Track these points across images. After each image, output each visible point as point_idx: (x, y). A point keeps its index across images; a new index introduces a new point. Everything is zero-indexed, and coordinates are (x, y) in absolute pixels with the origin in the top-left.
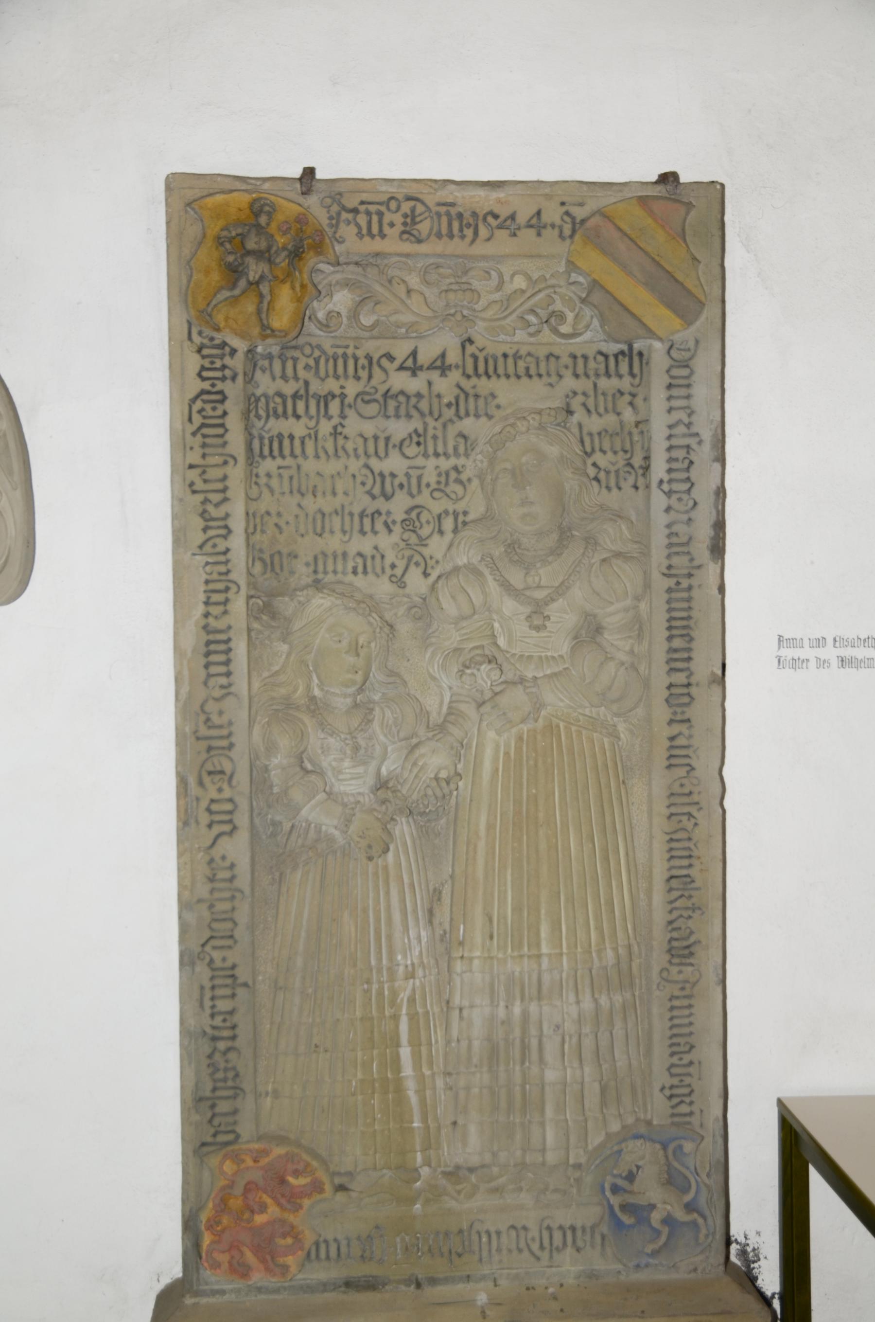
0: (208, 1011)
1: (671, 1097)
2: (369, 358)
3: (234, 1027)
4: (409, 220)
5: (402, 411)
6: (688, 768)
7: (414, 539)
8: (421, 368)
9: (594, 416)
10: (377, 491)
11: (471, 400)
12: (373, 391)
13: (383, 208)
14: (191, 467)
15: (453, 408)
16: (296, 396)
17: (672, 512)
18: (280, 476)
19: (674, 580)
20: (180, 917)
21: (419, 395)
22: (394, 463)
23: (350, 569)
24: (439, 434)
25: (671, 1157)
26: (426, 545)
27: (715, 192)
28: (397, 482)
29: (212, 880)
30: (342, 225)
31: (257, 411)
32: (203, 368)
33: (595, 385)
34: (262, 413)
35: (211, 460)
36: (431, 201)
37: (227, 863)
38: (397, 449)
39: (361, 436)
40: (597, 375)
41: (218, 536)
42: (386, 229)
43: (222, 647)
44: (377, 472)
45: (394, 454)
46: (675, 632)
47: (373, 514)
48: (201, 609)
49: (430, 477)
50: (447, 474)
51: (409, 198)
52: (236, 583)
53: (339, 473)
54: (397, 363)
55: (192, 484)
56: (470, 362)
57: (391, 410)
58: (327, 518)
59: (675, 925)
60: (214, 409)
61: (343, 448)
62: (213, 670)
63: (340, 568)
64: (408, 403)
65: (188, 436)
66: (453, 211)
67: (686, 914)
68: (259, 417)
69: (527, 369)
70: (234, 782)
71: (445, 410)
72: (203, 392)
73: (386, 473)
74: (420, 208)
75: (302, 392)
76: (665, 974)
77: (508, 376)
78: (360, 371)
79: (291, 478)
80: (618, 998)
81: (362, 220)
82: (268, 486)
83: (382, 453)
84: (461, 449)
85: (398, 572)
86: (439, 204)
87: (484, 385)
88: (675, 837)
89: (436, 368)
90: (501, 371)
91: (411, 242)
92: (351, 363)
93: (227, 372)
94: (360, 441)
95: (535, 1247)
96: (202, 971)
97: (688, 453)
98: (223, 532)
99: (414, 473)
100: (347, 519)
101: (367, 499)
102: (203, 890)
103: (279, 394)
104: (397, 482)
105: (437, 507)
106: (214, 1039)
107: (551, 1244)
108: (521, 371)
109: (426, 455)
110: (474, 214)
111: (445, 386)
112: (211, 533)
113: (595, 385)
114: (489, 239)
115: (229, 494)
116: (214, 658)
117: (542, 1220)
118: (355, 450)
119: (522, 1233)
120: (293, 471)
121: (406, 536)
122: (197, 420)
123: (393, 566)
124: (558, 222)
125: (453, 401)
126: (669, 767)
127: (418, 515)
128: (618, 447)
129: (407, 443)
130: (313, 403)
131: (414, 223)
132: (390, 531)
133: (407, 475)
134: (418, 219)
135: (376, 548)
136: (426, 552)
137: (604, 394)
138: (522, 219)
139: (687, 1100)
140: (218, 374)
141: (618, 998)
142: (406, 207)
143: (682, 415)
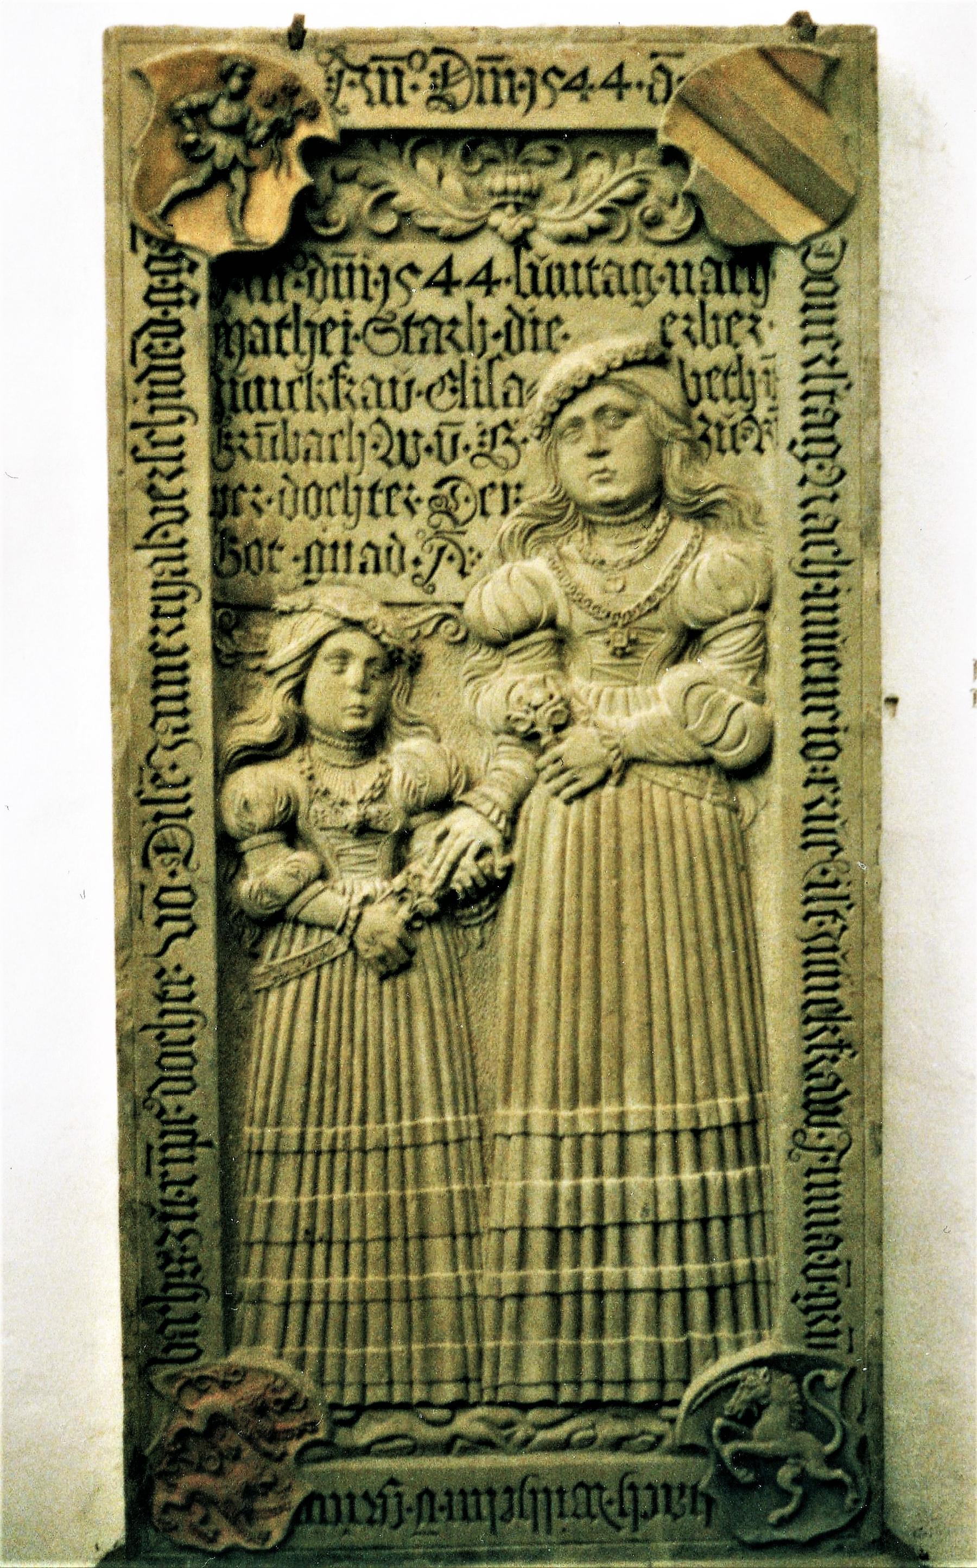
0: (158, 1180)
1: (806, 1311)
2: (384, 269)
3: (193, 1202)
4: (439, 81)
5: (431, 345)
6: (834, 848)
7: (446, 523)
8: (458, 283)
9: (701, 348)
10: (394, 455)
11: (528, 328)
12: (389, 317)
13: (403, 65)
14: (135, 425)
15: (502, 340)
16: (281, 324)
17: (808, 485)
18: (259, 435)
19: (813, 581)
20: (119, 1051)
21: (454, 322)
22: (421, 418)
23: (355, 565)
24: (483, 374)
25: (807, 1394)
26: (464, 533)
27: (863, 39)
28: (423, 443)
29: (162, 997)
30: (345, 90)
31: (228, 348)
32: (151, 290)
33: (702, 305)
34: (236, 349)
35: (160, 416)
36: (470, 53)
37: (183, 976)
38: (423, 398)
39: (372, 378)
40: (705, 291)
41: (171, 522)
42: (407, 94)
43: (177, 675)
44: (395, 430)
45: (419, 404)
46: (813, 654)
47: (389, 490)
48: (149, 623)
49: (469, 436)
50: (494, 431)
51: (437, 51)
52: (196, 587)
53: (341, 432)
54: (424, 278)
55: (135, 450)
56: (526, 275)
57: (415, 343)
58: (324, 494)
59: (814, 1070)
60: (166, 345)
61: (348, 396)
62: (163, 706)
63: (341, 563)
64: (439, 332)
65: (130, 382)
66: (501, 67)
67: (829, 1052)
68: (230, 354)
69: (607, 284)
70: (193, 864)
71: (490, 342)
72: (151, 322)
73: (408, 431)
74: (455, 64)
75: (291, 318)
76: (799, 1137)
77: (579, 293)
78: (372, 288)
79: (274, 438)
80: (734, 1175)
81: (373, 81)
82: (241, 448)
83: (401, 401)
84: (514, 398)
85: (425, 569)
86: (481, 58)
87: (545, 307)
88: (813, 944)
89: (480, 283)
90: (569, 285)
91: (443, 112)
92: (358, 276)
93: (186, 295)
94: (371, 386)
95: (613, 1510)
96: (150, 1126)
97: (832, 402)
98: (177, 515)
99: (448, 432)
100: (353, 495)
101: (382, 468)
102: (150, 1012)
103: (258, 321)
104: (423, 443)
105: (479, 479)
106: (166, 1217)
107: (636, 1510)
108: (599, 286)
109: (463, 405)
110: (530, 71)
111: (493, 309)
112: (161, 517)
113: (702, 305)
114: (551, 106)
115: (185, 462)
116: (164, 691)
117: (626, 1474)
118: (365, 399)
119: (595, 1494)
120: (278, 428)
121: (435, 519)
122: (143, 361)
123: (417, 562)
124: (648, 80)
125: (503, 330)
126: (805, 846)
127: (453, 489)
128: (734, 390)
129: (436, 390)
130: (305, 334)
131: (445, 84)
132: (413, 512)
133: (439, 434)
134: (452, 80)
135: (393, 536)
136: (465, 542)
137: (715, 317)
138: (596, 76)
139: (831, 1313)
140: (173, 296)
141: (734, 1175)
142: (435, 63)
143: (822, 347)
